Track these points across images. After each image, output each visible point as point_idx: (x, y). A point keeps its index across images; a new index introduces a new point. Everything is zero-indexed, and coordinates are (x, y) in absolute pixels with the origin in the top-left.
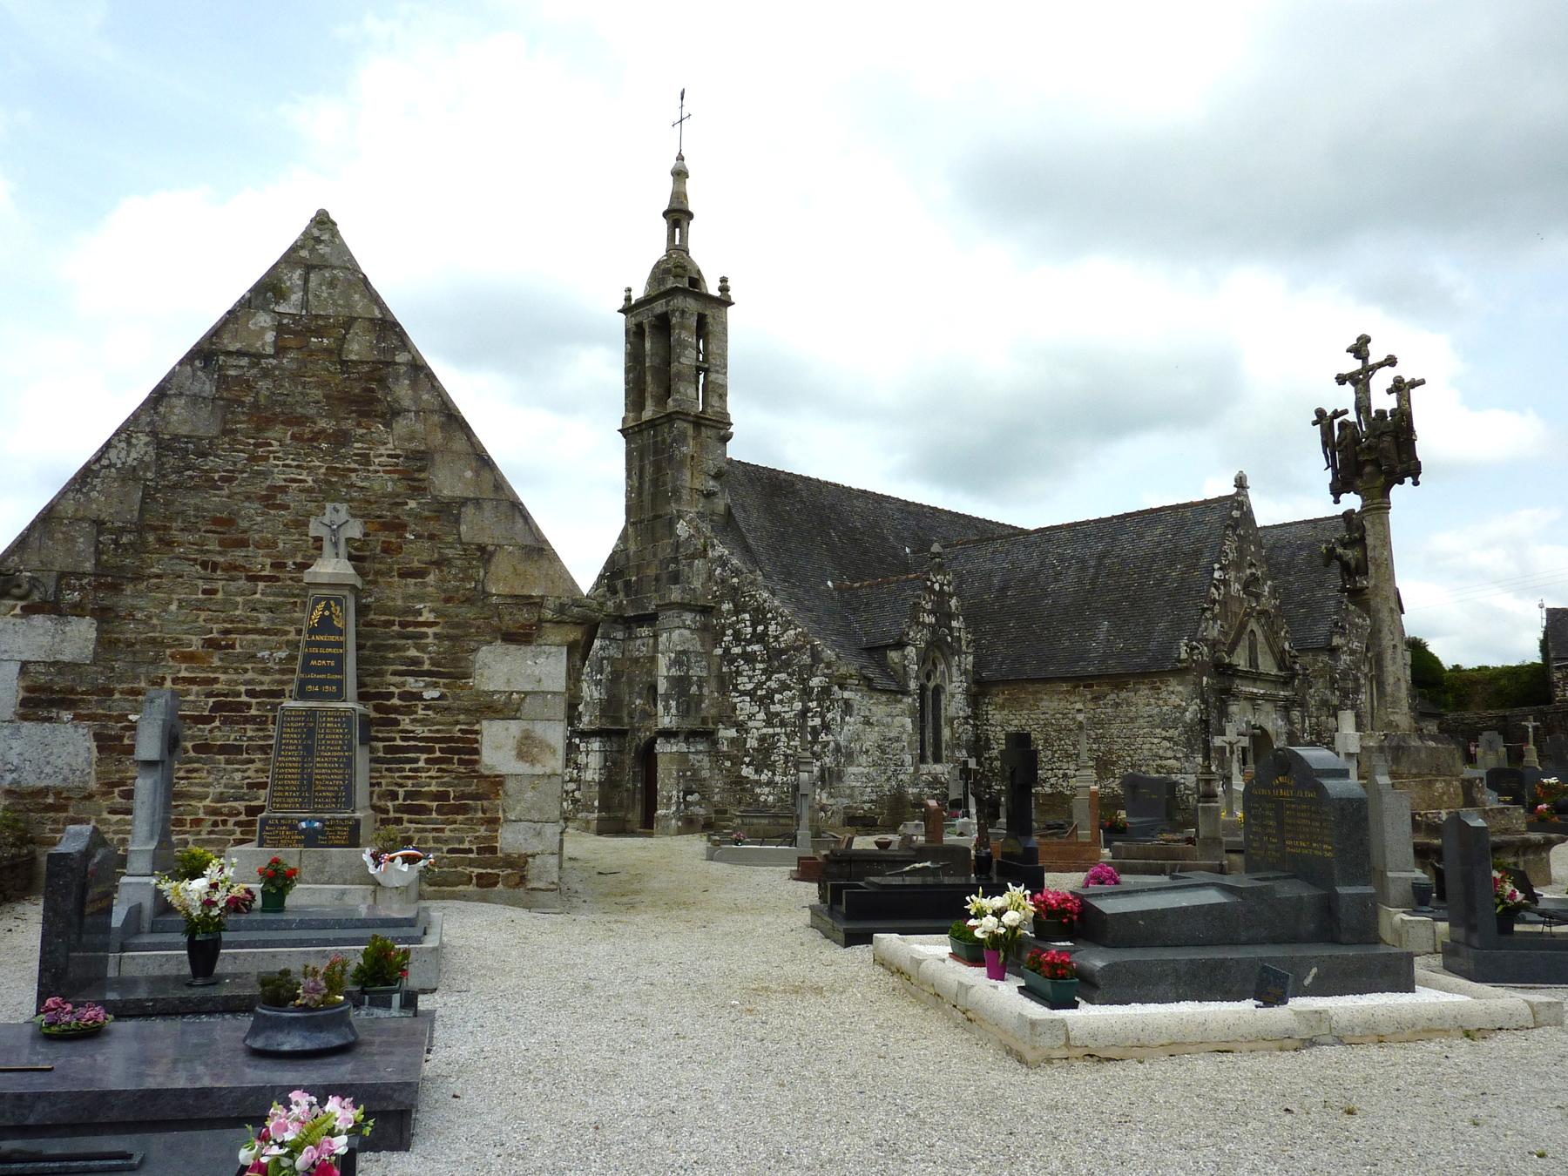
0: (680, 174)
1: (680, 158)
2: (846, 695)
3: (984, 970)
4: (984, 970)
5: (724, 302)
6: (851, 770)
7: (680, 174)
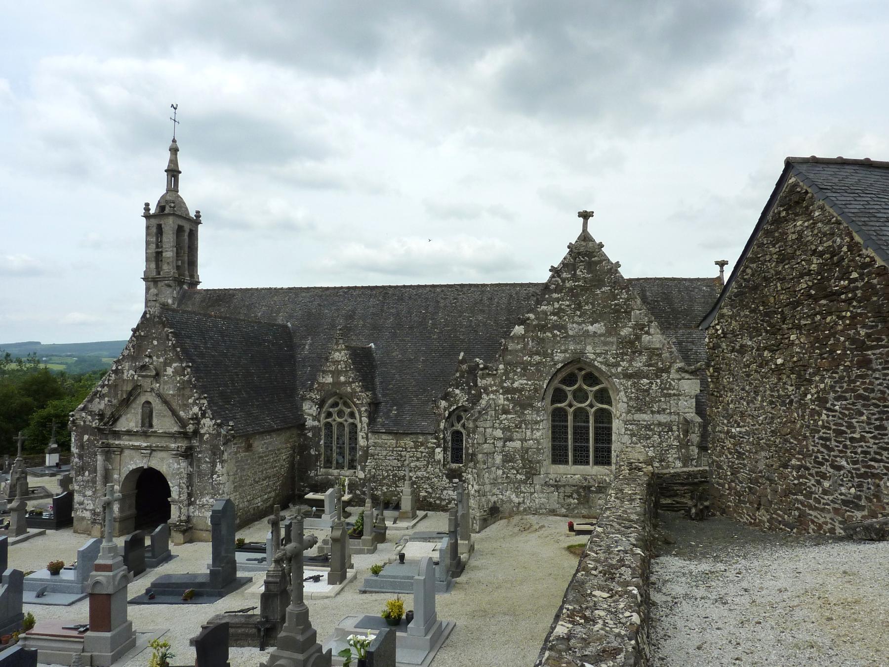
1: (174, 141)
5: (197, 221)
7: (174, 150)
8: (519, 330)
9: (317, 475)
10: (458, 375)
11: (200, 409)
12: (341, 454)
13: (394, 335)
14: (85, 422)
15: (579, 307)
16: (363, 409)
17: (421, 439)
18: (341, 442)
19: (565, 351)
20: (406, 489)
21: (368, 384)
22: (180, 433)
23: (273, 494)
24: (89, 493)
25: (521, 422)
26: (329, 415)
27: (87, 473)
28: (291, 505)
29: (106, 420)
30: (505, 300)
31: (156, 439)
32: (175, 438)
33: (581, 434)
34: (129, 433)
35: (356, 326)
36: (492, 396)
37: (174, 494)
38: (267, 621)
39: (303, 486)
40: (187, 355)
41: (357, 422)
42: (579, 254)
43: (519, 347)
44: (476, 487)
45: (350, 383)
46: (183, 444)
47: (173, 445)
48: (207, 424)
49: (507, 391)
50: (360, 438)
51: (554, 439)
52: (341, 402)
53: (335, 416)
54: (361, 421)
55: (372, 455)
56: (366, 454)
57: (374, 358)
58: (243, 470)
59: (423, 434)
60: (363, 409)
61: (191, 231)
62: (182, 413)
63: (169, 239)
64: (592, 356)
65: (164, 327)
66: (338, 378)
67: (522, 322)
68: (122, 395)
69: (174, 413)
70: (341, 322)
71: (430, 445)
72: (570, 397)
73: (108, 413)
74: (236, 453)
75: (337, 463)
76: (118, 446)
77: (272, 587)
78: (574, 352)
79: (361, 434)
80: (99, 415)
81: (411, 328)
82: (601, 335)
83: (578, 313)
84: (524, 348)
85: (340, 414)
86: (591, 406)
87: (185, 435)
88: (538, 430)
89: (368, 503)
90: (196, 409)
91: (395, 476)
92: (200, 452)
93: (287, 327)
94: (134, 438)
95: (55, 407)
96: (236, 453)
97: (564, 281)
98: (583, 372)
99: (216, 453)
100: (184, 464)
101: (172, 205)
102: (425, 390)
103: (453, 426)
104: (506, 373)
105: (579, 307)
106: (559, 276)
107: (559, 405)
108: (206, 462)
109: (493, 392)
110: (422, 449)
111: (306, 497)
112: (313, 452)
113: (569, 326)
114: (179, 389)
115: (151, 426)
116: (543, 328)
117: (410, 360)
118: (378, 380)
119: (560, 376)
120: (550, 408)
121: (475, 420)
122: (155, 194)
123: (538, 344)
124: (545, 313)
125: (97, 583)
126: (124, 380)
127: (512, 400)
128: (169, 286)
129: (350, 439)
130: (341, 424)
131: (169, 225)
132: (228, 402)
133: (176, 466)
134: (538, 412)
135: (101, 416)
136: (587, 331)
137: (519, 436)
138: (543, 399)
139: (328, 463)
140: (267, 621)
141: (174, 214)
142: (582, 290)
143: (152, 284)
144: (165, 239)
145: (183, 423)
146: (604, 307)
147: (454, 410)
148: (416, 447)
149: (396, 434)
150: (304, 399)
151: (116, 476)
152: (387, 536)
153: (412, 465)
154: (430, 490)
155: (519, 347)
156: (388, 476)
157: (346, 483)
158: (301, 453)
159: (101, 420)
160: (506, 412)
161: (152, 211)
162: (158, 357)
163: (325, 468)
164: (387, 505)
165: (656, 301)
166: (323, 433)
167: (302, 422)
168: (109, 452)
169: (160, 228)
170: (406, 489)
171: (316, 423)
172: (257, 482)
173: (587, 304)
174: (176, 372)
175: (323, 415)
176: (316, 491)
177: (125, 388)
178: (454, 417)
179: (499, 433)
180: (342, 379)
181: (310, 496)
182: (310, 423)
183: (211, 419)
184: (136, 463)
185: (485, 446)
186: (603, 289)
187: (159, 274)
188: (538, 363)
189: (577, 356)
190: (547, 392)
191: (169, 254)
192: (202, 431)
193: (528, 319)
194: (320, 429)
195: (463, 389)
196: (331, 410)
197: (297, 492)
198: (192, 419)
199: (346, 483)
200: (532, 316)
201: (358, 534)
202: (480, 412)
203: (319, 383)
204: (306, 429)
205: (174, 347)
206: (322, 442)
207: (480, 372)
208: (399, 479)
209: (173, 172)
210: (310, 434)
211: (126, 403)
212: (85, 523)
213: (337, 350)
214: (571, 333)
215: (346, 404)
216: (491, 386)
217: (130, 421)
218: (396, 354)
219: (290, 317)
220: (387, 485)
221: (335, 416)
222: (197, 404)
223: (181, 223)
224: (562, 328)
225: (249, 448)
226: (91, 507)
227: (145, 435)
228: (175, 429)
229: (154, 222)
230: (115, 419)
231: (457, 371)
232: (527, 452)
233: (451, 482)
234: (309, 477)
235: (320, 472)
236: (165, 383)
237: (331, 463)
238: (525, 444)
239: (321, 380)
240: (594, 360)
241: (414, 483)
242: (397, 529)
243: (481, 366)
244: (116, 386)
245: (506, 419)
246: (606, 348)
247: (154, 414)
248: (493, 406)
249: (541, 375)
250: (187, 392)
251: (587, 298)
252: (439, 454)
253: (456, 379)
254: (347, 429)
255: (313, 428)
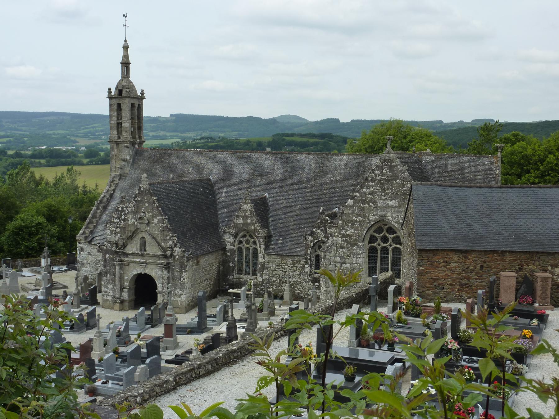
0: (126, 48)
1: (126, 41)
2: (81, 245)
3: (341, 121)
4: (341, 121)
5: (142, 98)
6: (83, 269)
7: (126, 48)
8: (350, 202)
9: (233, 278)
10: (319, 221)
11: (173, 242)
12: (248, 266)
13: (281, 188)
14: (106, 247)
15: (384, 191)
16: (261, 240)
17: (296, 259)
18: (247, 259)
19: (376, 215)
20: (286, 288)
21: (265, 223)
22: (163, 255)
23: (209, 289)
24: (110, 286)
25: (351, 253)
26: (240, 242)
27: (109, 276)
28: (218, 296)
29: (120, 247)
30: (355, 166)
31: (149, 258)
32: (159, 258)
33: (384, 260)
34: (133, 254)
35: (256, 181)
36: (335, 238)
37: (160, 288)
38: (229, 337)
39: (225, 285)
40: (164, 212)
41: (258, 247)
42: (385, 160)
43: (350, 211)
44: (325, 288)
45: (254, 224)
46: (164, 262)
47: (158, 262)
48: (178, 251)
49: (343, 236)
50: (259, 257)
51: (369, 263)
52: (248, 235)
53: (244, 243)
54: (260, 247)
55: (267, 268)
56: (263, 267)
57: (268, 204)
58: (195, 276)
59: (298, 256)
60: (261, 240)
61: (139, 105)
62: (163, 244)
63: (126, 113)
64: (390, 219)
65: (152, 196)
66: (246, 220)
67: (353, 198)
68: (128, 233)
69: (159, 245)
70: (246, 177)
71: (302, 263)
72: (379, 240)
73: (121, 243)
74: (192, 266)
75: (246, 271)
76: (126, 261)
77: (231, 325)
78: (381, 216)
79: (260, 255)
80: (116, 244)
81: (292, 183)
82: (396, 207)
83: (384, 194)
84: (353, 212)
85: (248, 242)
86: (391, 246)
87: (165, 257)
88: (360, 258)
89: (266, 296)
90: (171, 242)
91: (280, 280)
92: (174, 266)
93: (209, 179)
94: (136, 257)
95: (22, 220)
96: (192, 266)
97: (376, 176)
98: (386, 227)
99: (182, 267)
100: (165, 272)
101: (128, 90)
102: (300, 228)
103: (316, 251)
104: (343, 226)
105: (384, 191)
106: (373, 173)
107: (373, 244)
108: (177, 271)
109: (335, 236)
110: (297, 265)
111: (229, 291)
112: (231, 264)
113: (378, 201)
114: (161, 231)
115: (145, 250)
116: (364, 202)
117: (292, 206)
118: (271, 219)
119: (374, 228)
120: (368, 246)
121: (325, 252)
122: (114, 77)
123: (361, 210)
124: (365, 193)
125: (168, 320)
126: (129, 225)
127: (346, 241)
128: (128, 147)
129: (253, 257)
130: (248, 249)
131: (126, 104)
132: (186, 237)
133: (160, 273)
134: (360, 248)
135: (117, 245)
136: (388, 204)
137: (349, 261)
138: (363, 241)
139: (240, 271)
140: (229, 337)
141: (129, 97)
142: (386, 181)
143: (115, 145)
144: (123, 114)
145: (164, 250)
146: (398, 191)
147: (317, 242)
148: (293, 264)
149: (281, 256)
150: (225, 232)
151: (126, 278)
152: (276, 313)
153: (291, 274)
154: (301, 289)
155: (350, 211)
156: (277, 280)
157: (252, 284)
158: (223, 265)
159: (117, 246)
160: (342, 247)
161: (113, 94)
162: (148, 213)
163: (238, 274)
164: (276, 297)
165: (454, 171)
166: (237, 253)
167: (224, 246)
168: (122, 264)
169: (119, 106)
170: (286, 288)
171: (233, 247)
172: (202, 282)
173: (388, 189)
174: (159, 222)
175: (237, 242)
176: (234, 288)
177: (129, 229)
178: (316, 247)
179: (338, 259)
180: (249, 221)
181: (231, 290)
182: (229, 247)
183: (180, 248)
184: (137, 271)
185: (330, 266)
186: (398, 181)
187: (119, 138)
188: (361, 221)
189: (382, 218)
190: (366, 237)
191: (126, 125)
192: (175, 255)
193: (356, 196)
194: (235, 251)
195: (322, 230)
196: (242, 239)
197: (221, 288)
198: (169, 248)
199: (252, 284)
200: (358, 194)
201: (261, 310)
202: (327, 247)
203: (234, 223)
204: (226, 251)
205: (158, 207)
206: (236, 259)
207: (329, 225)
208: (283, 282)
209: (126, 65)
210: (229, 254)
211: (131, 237)
212: (108, 302)
213: (246, 203)
214: (379, 205)
215: (251, 236)
216: (334, 233)
217: (133, 247)
218: (283, 202)
219: (212, 171)
220: (276, 285)
221: (244, 243)
222: (172, 240)
223: (133, 102)
224: (374, 202)
225: (198, 263)
226: (112, 294)
227: (142, 255)
228: (159, 253)
229: (115, 102)
230: (124, 246)
231: (318, 219)
232: (353, 270)
233: (314, 284)
234: (229, 279)
235: (235, 277)
236: (153, 227)
237: (242, 271)
238: (353, 266)
239: (236, 221)
240: (392, 221)
241: (292, 285)
242: (281, 310)
243: (329, 221)
244: (124, 228)
245: (342, 251)
246: (398, 214)
247: (147, 244)
248: (335, 244)
249: (362, 228)
250: (166, 233)
251: (389, 186)
252: (307, 268)
253: (318, 224)
254: (251, 251)
255: (231, 250)
